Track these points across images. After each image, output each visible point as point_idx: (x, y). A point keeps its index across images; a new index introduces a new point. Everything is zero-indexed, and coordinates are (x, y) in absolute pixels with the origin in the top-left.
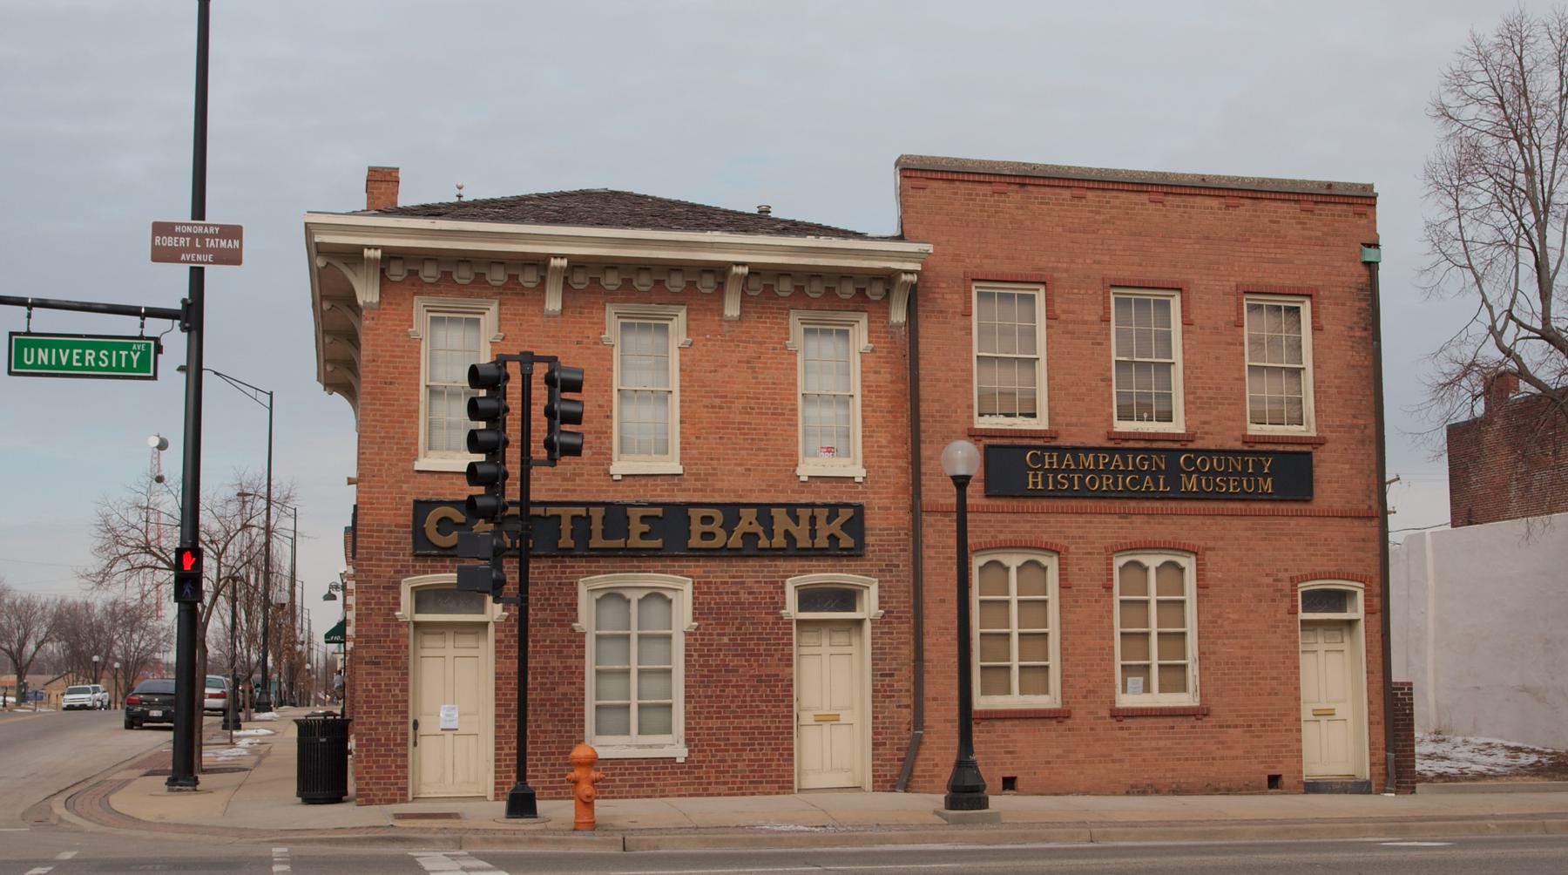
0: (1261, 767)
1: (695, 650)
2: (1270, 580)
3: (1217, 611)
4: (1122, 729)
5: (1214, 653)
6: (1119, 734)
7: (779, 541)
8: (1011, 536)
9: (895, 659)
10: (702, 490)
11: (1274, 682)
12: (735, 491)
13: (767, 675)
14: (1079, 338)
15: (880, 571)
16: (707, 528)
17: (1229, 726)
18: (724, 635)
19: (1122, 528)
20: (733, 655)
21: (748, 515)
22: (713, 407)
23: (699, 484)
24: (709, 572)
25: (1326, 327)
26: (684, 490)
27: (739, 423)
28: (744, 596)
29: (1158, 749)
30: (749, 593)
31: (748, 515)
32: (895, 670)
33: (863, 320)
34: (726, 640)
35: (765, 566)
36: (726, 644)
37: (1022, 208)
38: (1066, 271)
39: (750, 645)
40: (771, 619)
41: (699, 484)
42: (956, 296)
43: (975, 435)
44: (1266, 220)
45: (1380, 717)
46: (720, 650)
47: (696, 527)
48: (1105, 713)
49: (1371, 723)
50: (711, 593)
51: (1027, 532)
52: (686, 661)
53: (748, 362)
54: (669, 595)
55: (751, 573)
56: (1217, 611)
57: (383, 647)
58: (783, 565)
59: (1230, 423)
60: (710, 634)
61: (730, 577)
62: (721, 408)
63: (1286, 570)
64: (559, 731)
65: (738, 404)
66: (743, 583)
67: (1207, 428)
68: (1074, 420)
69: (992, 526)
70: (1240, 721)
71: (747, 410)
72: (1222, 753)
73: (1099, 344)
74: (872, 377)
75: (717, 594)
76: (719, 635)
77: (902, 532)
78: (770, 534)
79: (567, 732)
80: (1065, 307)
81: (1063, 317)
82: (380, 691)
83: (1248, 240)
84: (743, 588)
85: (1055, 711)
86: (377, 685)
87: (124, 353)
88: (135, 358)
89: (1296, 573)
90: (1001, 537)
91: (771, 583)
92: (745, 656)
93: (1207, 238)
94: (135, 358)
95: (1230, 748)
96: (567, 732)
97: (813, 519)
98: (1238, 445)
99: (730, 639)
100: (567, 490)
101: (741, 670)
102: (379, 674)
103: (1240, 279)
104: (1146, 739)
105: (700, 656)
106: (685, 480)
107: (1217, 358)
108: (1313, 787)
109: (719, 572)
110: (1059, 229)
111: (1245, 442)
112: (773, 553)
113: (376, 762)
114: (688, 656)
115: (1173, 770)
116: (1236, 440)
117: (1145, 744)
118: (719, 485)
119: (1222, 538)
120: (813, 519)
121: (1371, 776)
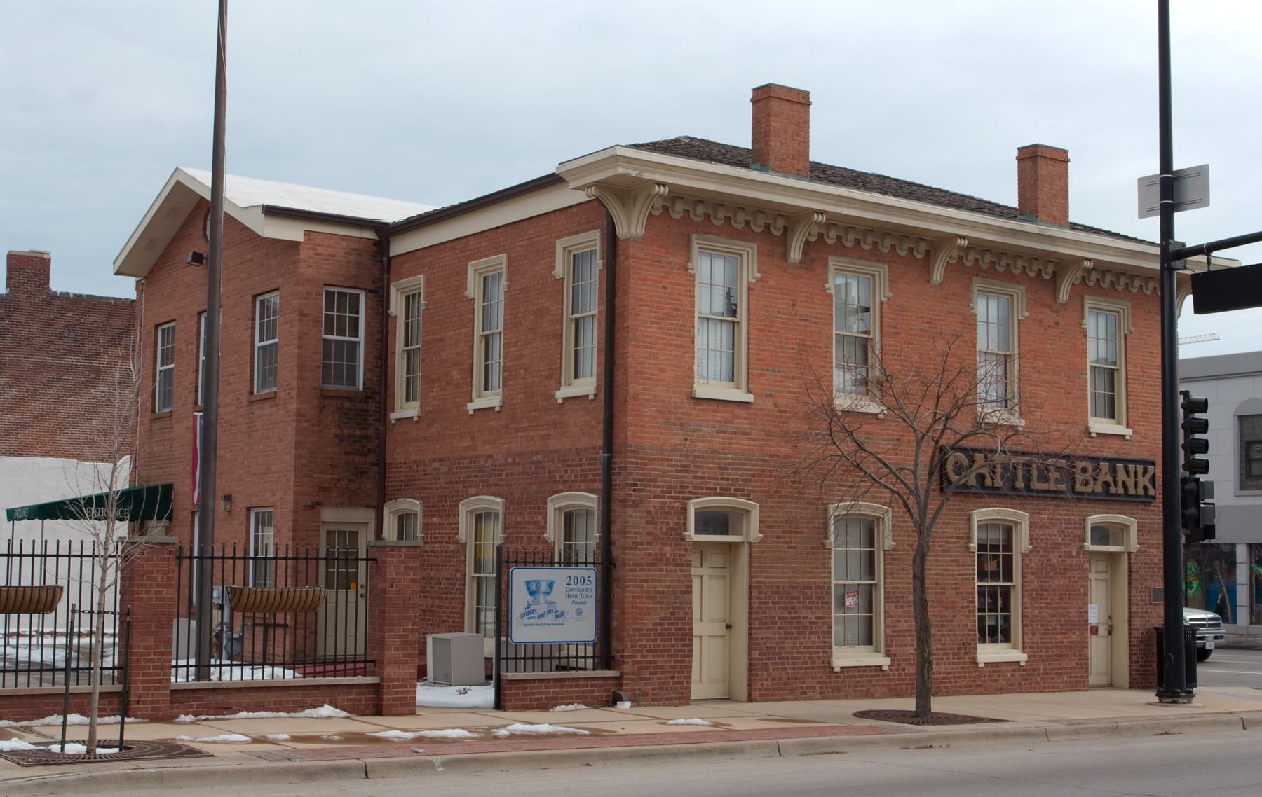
21: (1105, 466)
55: (1067, 512)
109: (1049, 511)
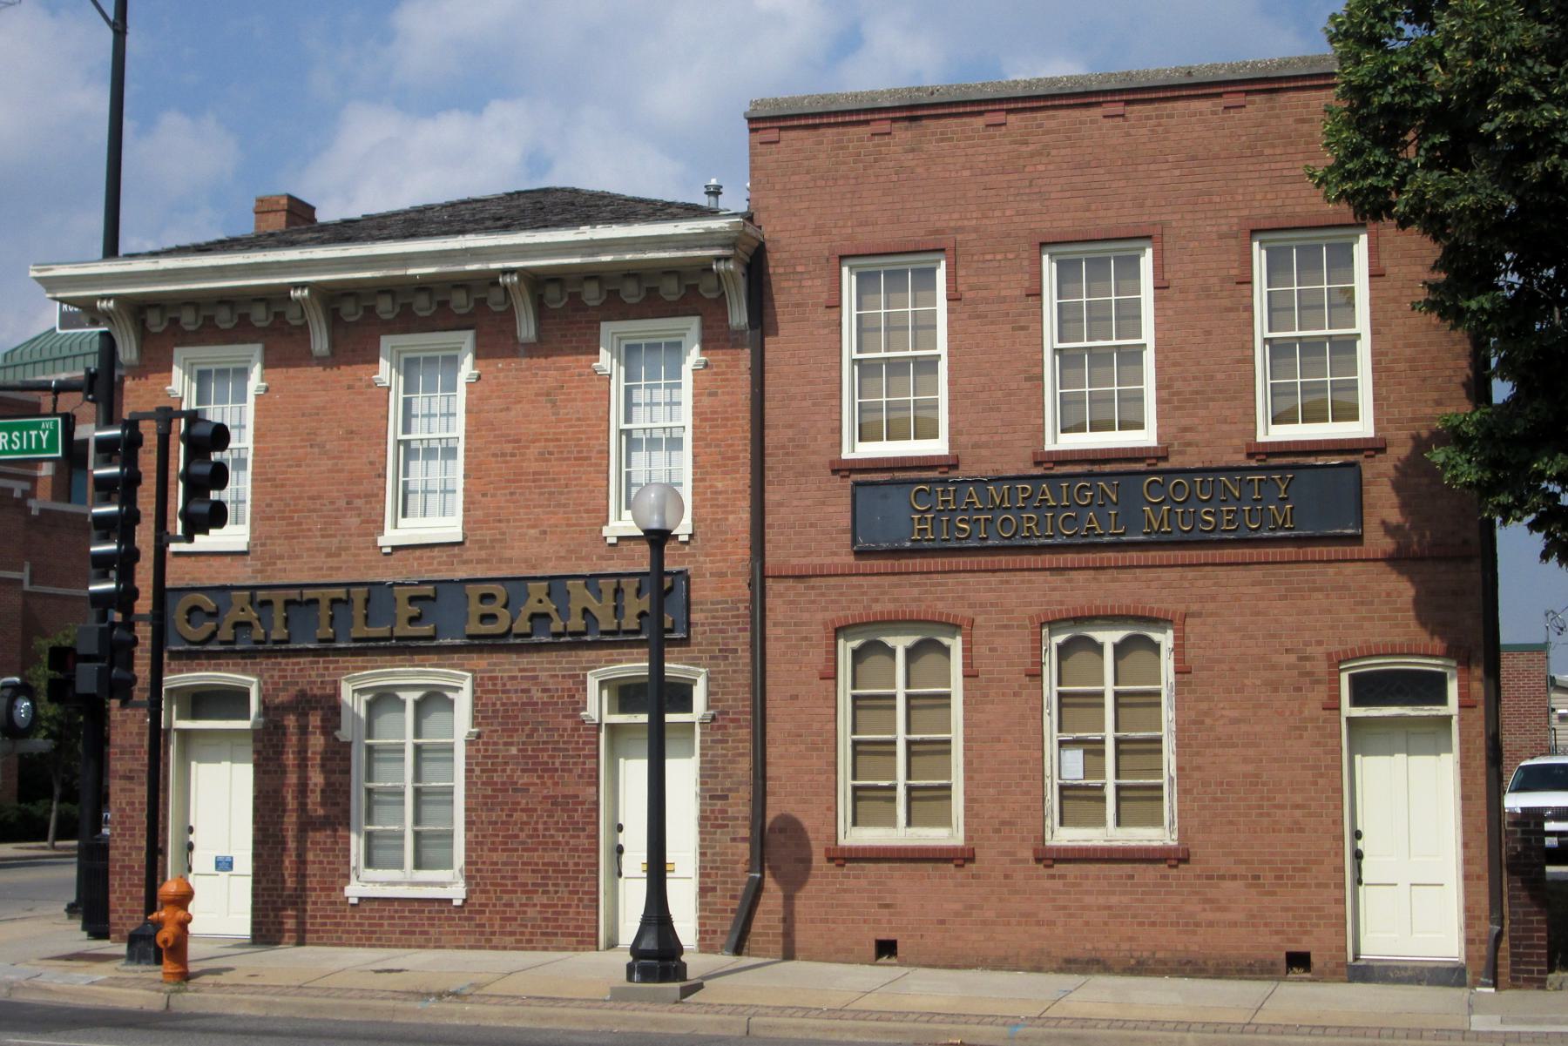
0: (1276, 939)
1: (477, 764)
2: (1292, 658)
3: (1204, 706)
4: (1053, 877)
5: (1199, 768)
6: (1048, 884)
7: (576, 623)
8: (891, 607)
9: (730, 776)
10: (486, 561)
11: (1298, 813)
12: (526, 561)
13: (564, 797)
14: (992, 323)
15: (712, 658)
16: (487, 608)
17: (1222, 877)
18: (512, 744)
19: (1054, 589)
20: (524, 771)
21: (537, 590)
22: (504, 455)
23: (483, 554)
24: (495, 664)
25: (1389, 270)
26: (465, 562)
27: (535, 473)
28: (537, 695)
29: (1109, 908)
30: (545, 691)
31: (537, 590)
32: (730, 790)
33: (693, 325)
34: (514, 750)
35: (624, 654)
36: (513, 757)
37: (913, 150)
38: (976, 230)
39: (544, 757)
40: (569, 723)
41: (483, 554)
42: (818, 282)
43: (844, 469)
44: (1291, 120)
45: (1481, 867)
46: (506, 764)
47: (476, 608)
48: (1028, 854)
49: (1467, 877)
50: (496, 692)
51: (915, 600)
52: (466, 778)
53: (548, 394)
54: (450, 695)
56: (1204, 706)
57: (137, 759)
58: (587, 655)
59: (1225, 427)
60: (495, 744)
61: (521, 670)
62: (513, 455)
63: (1320, 643)
64: (321, 862)
65: (533, 450)
66: (536, 678)
67: (1189, 436)
68: (984, 438)
69: (864, 594)
70: (1241, 869)
71: (543, 457)
72: (1210, 916)
73: (1022, 328)
74: (706, 401)
75: (504, 692)
76: (506, 744)
77: (741, 606)
78: (564, 613)
79: (329, 863)
80: (973, 280)
81: (968, 295)
82: (134, 810)
83: (1261, 154)
84: (536, 684)
85: (954, 849)
86: (132, 804)
87: (33, 433)
88: (44, 438)
89: (1336, 647)
90: (877, 607)
91: (571, 676)
92: (536, 770)
93: (1194, 158)
94: (44, 438)
95: (1224, 909)
96: (329, 863)
97: (618, 591)
98: (1240, 459)
99: (519, 750)
100: (331, 568)
101: (532, 789)
102: (132, 791)
103: (1245, 213)
104: (1087, 893)
105: (483, 771)
106: (468, 550)
107: (1208, 333)
108: (1364, 973)
109: (507, 666)
110: (966, 173)
111: (1250, 455)
112: (576, 642)
113: (129, 893)
114: (469, 771)
115: (1131, 939)
116: (1236, 451)
117: (1088, 900)
118: (508, 554)
119: (1213, 598)
120: (618, 591)
121: (1468, 958)
